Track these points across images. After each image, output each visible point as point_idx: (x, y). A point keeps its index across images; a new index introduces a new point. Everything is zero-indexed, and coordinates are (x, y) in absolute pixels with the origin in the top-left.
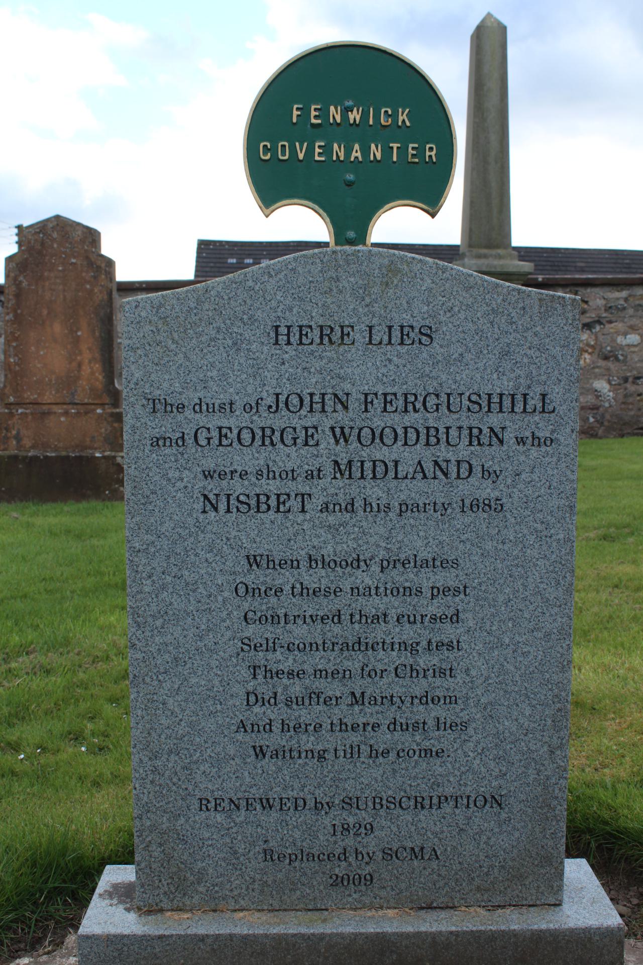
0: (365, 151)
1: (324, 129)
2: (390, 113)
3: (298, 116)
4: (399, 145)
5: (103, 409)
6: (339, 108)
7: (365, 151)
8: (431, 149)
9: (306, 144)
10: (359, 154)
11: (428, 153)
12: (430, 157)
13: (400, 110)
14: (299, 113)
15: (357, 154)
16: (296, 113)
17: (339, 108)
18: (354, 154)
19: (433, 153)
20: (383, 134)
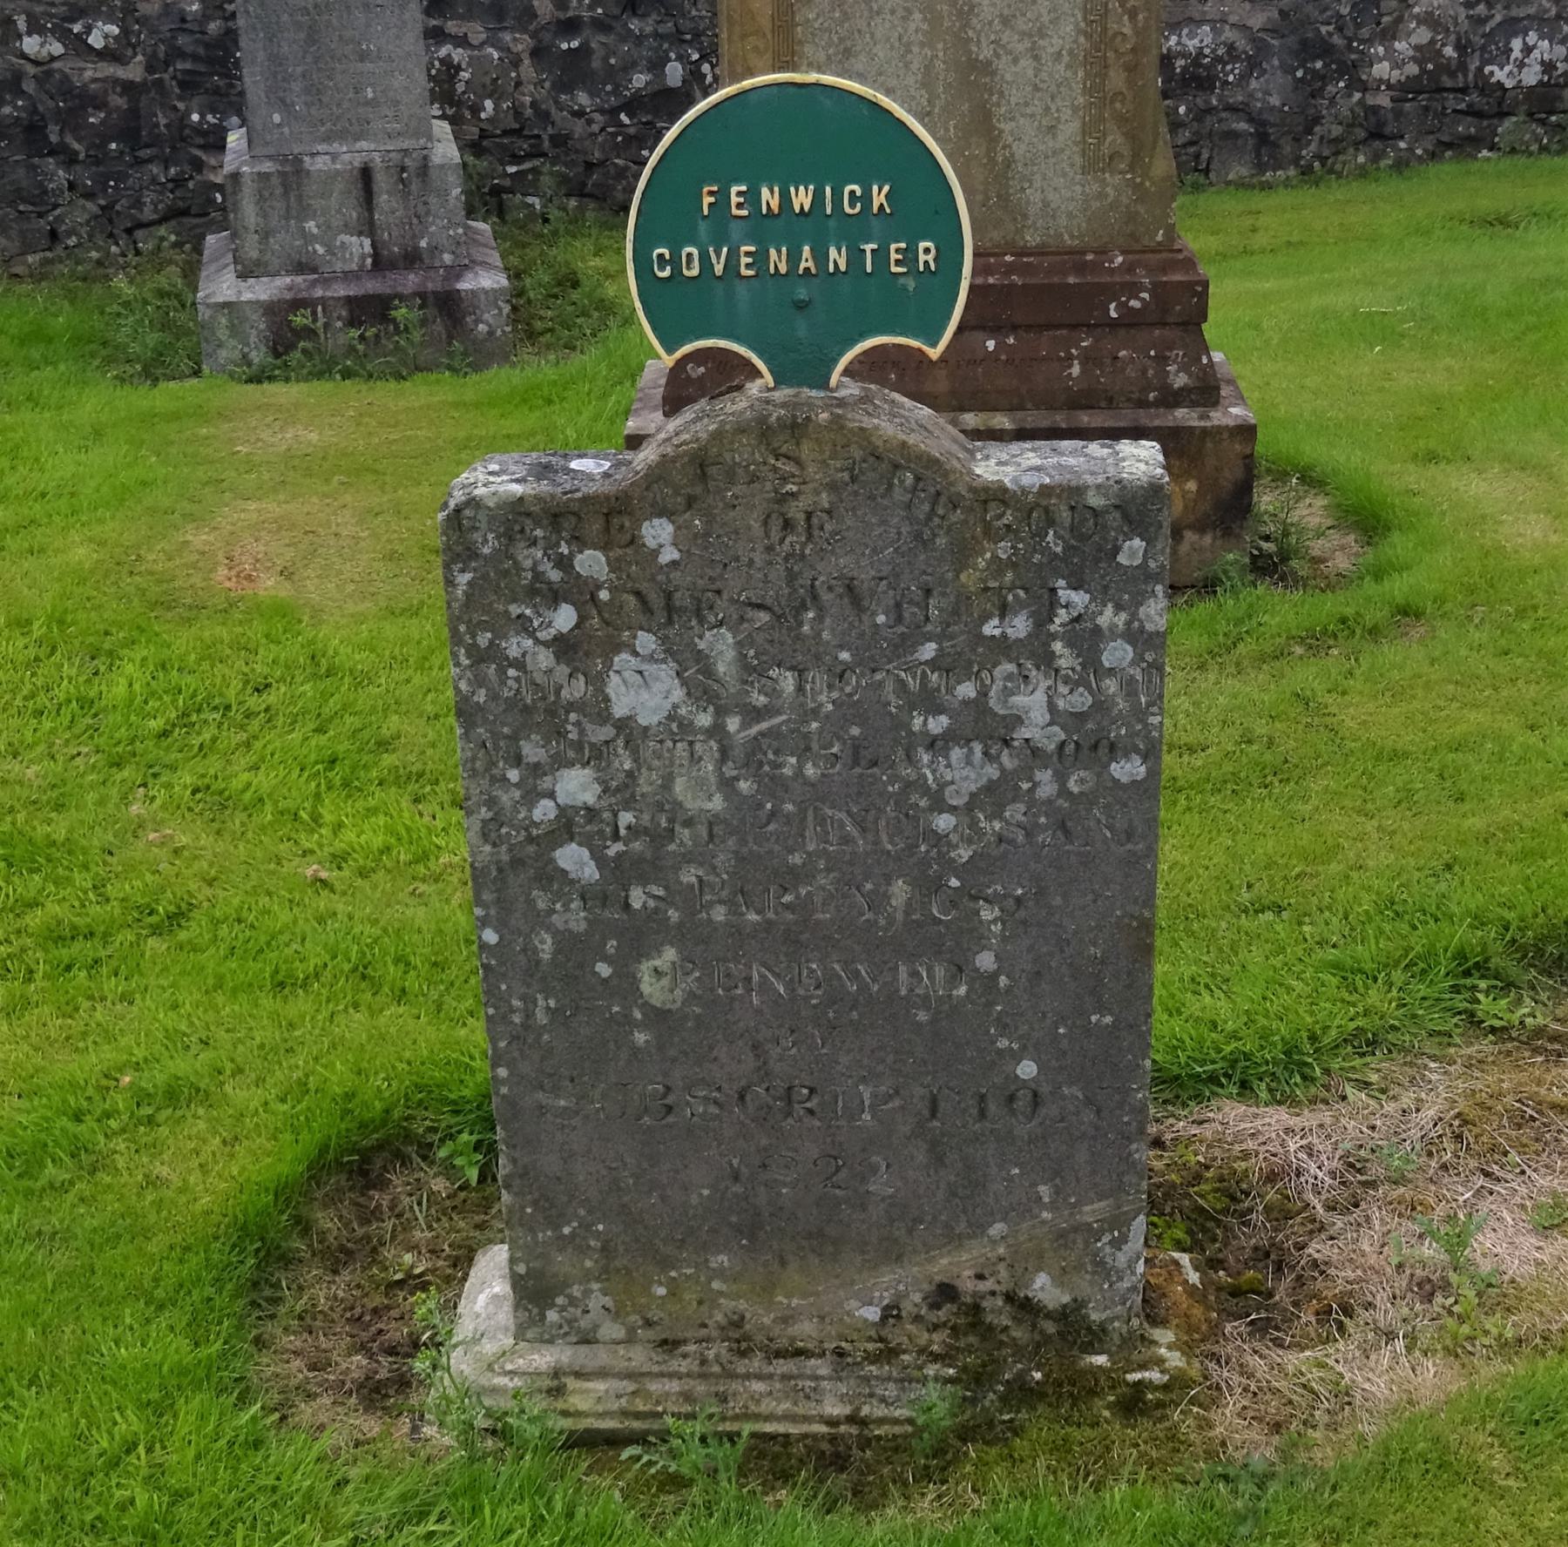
0: (820, 256)
1: (763, 226)
2: (859, 193)
3: (710, 204)
4: (875, 246)
5: (929, 638)
6: (776, 189)
7: (820, 256)
8: (927, 251)
9: (725, 250)
10: (810, 264)
11: (922, 257)
12: (926, 262)
13: (792, 189)
14: (712, 199)
15: (807, 262)
16: (707, 200)
17: (776, 189)
18: (803, 265)
19: (930, 258)
20: (853, 230)
